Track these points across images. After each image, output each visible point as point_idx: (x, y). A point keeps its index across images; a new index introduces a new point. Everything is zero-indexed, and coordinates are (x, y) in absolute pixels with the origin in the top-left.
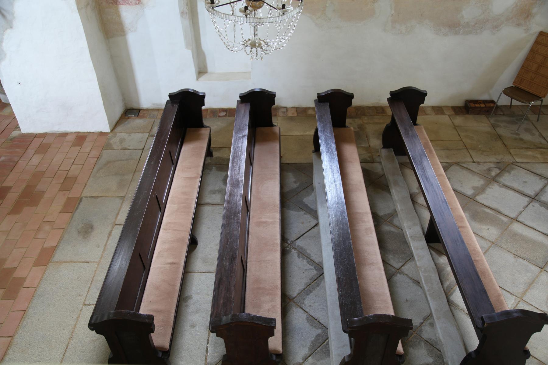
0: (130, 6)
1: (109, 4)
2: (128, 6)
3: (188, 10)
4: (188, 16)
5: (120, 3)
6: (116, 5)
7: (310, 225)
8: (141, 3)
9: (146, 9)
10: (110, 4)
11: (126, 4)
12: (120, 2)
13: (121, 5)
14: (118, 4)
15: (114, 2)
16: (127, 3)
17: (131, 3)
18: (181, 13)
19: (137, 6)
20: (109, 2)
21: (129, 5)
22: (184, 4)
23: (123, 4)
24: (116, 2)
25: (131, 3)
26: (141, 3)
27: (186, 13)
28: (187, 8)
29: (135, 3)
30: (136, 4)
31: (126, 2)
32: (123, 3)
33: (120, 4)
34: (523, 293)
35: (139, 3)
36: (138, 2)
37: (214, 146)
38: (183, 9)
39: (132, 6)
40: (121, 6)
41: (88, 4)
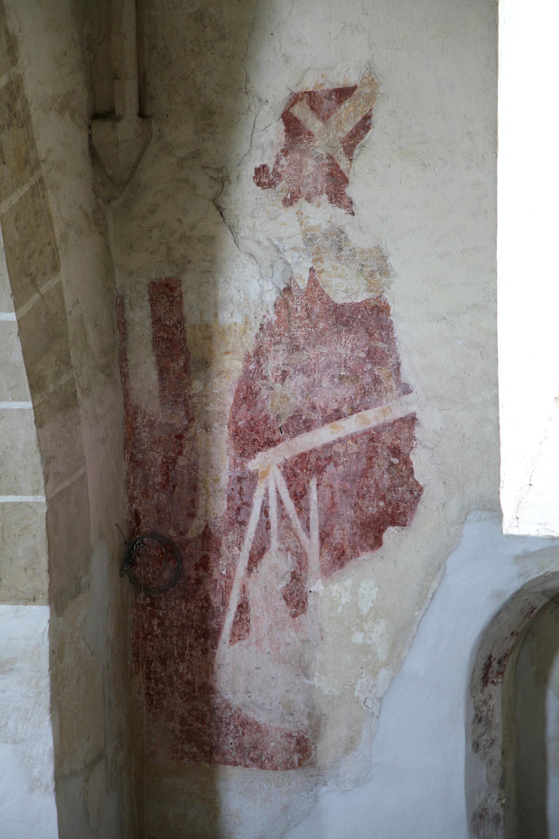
0: (263, 772)
1: (182, 759)
2: (255, 771)
3: (503, 805)
4: (501, 832)
5: (227, 757)
6: (207, 765)
7: (220, 704)
8: (312, 764)
9: (324, 789)
10: (186, 760)
11: (248, 762)
12: (224, 755)
13: (229, 767)
14: (218, 762)
15: (204, 751)
16: (253, 760)
17: (271, 758)
18: (474, 818)
19: (292, 772)
20: (182, 750)
21: (262, 767)
22: (488, 780)
23: (235, 764)
24: (211, 753)
25: (271, 758)
26: (312, 764)
27: (497, 818)
28: (499, 799)
29: (287, 762)
30: (288, 765)
31: (252, 755)
32: (238, 760)
33: (226, 763)
34: (364, 148)
35: (300, 765)
36: (300, 760)
37: (35, 609)
38: (486, 799)
39: (271, 774)
40: (230, 770)
41: (100, 756)
